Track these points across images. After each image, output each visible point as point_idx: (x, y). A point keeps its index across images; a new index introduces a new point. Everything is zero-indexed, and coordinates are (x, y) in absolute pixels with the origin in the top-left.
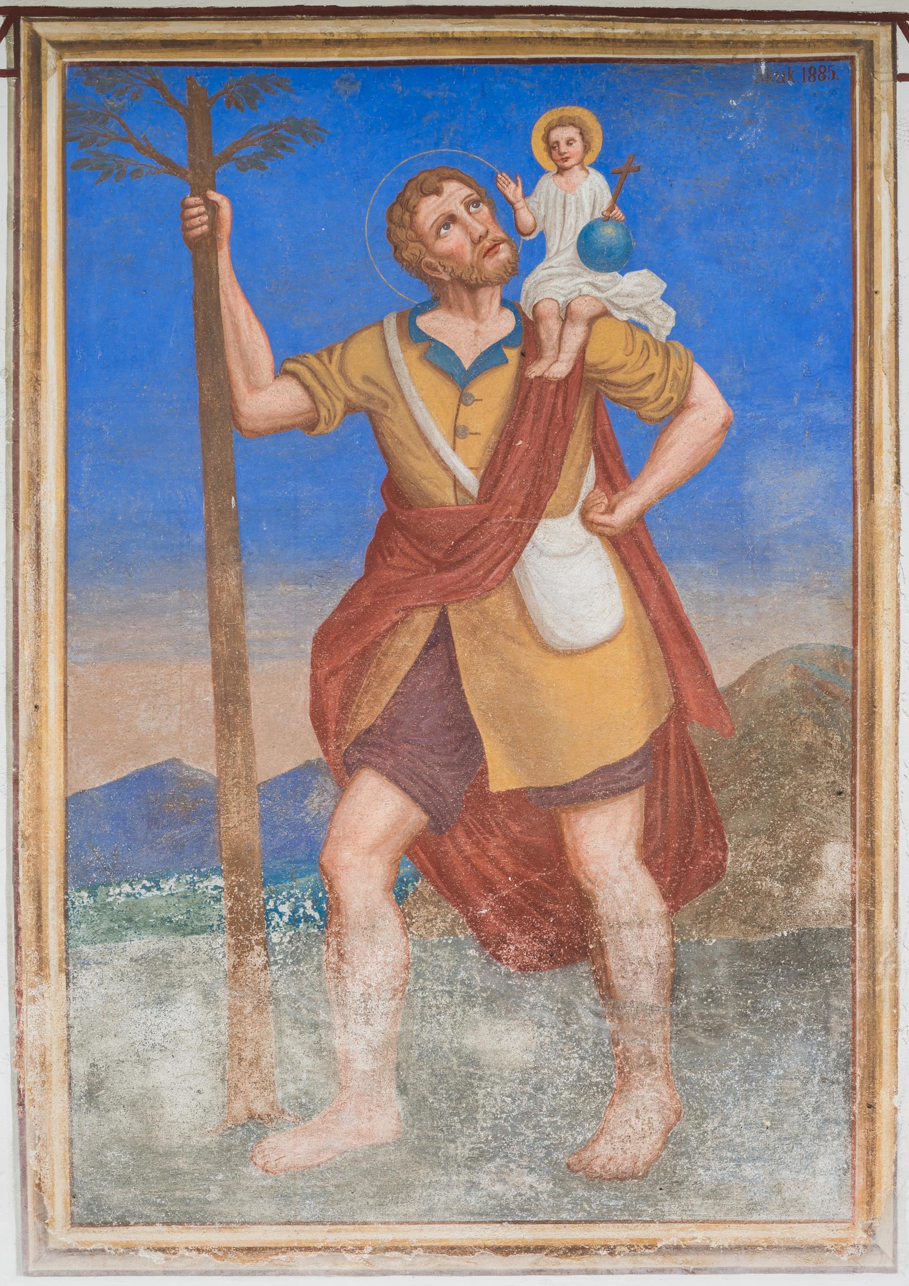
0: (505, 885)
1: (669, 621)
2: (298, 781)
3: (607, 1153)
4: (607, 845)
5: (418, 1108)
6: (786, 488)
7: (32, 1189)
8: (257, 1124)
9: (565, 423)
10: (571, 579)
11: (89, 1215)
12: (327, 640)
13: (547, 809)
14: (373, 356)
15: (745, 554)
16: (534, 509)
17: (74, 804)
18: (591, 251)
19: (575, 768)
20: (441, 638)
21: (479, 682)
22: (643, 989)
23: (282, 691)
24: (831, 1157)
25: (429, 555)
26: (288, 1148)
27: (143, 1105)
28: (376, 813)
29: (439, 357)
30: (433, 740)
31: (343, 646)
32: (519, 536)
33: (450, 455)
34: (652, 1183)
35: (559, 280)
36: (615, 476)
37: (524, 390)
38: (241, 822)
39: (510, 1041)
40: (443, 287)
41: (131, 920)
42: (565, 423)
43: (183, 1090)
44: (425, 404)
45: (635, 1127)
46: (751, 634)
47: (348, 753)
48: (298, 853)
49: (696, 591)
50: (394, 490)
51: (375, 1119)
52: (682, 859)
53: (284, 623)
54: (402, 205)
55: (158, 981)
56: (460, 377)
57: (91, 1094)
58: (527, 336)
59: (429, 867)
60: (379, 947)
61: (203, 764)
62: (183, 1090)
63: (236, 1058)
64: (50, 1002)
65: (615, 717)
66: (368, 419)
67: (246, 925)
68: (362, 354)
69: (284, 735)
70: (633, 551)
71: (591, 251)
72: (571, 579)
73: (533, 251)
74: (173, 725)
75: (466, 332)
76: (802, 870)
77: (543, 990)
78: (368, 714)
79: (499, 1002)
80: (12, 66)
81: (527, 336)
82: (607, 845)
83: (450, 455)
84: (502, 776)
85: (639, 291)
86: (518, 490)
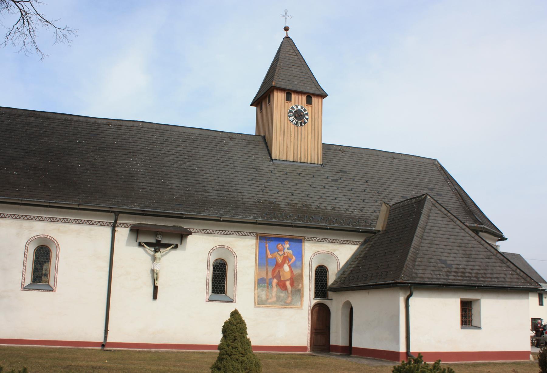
0: (282, 286)
1: (333, 209)
2: (271, 279)
3: (288, 302)
4: (288, 283)
5: (277, 299)
6: (298, 263)
7: (255, 302)
8: (268, 299)
9: (286, 259)
10: (286, 268)
11: (258, 304)
12: (273, 271)
13: (285, 281)
14: (276, 254)
15: (296, 267)
16: (284, 264)
17: (258, 280)
18: (288, 249)
19: (286, 279)
20: (279, 271)
21: (281, 274)
22: (290, 292)
23: (270, 273)
24: (300, 302)
25: (278, 266)
26: (270, 301)
27: (261, 298)
28: (275, 281)
29: (279, 254)
30: (278, 277)
31: (273, 271)
32: (283, 265)
33: (280, 260)
34: (290, 304)
35: (286, 250)
36: (289, 262)
37: (284, 257)
38: (267, 281)
39: (282, 295)
40: (280, 250)
41: (261, 286)
42: (286, 259)
43: (264, 297)
44: (278, 257)
45: (289, 300)
46: (296, 272)
47: (274, 277)
48: (271, 283)
49: (293, 269)
50: (277, 262)
51: (274, 299)
52: (292, 285)
53: (270, 269)
54: (277, 246)
55: (262, 290)
56: (280, 256)
57: (258, 297)
58: (284, 254)
59: (278, 284)
60: (275, 289)
61: (265, 278)
62: (264, 297)
63: (267, 295)
64: (256, 291)
65: (288, 276)
66: (275, 258)
67: (268, 287)
68: (275, 254)
69: (270, 276)
70: (290, 266)
71: (288, 249)
72: (286, 268)
73: (285, 249)
74: (264, 275)
75: (281, 253)
76: (298, 286)
77: (284, 292)
78: (275, 275)
79: (282, 292)
80: (113, 214)
81: (284, 254)
82: (288, 283)
83: (280, 260)
84: (282, 279)
85: (290, 251)
86: (283, 263)
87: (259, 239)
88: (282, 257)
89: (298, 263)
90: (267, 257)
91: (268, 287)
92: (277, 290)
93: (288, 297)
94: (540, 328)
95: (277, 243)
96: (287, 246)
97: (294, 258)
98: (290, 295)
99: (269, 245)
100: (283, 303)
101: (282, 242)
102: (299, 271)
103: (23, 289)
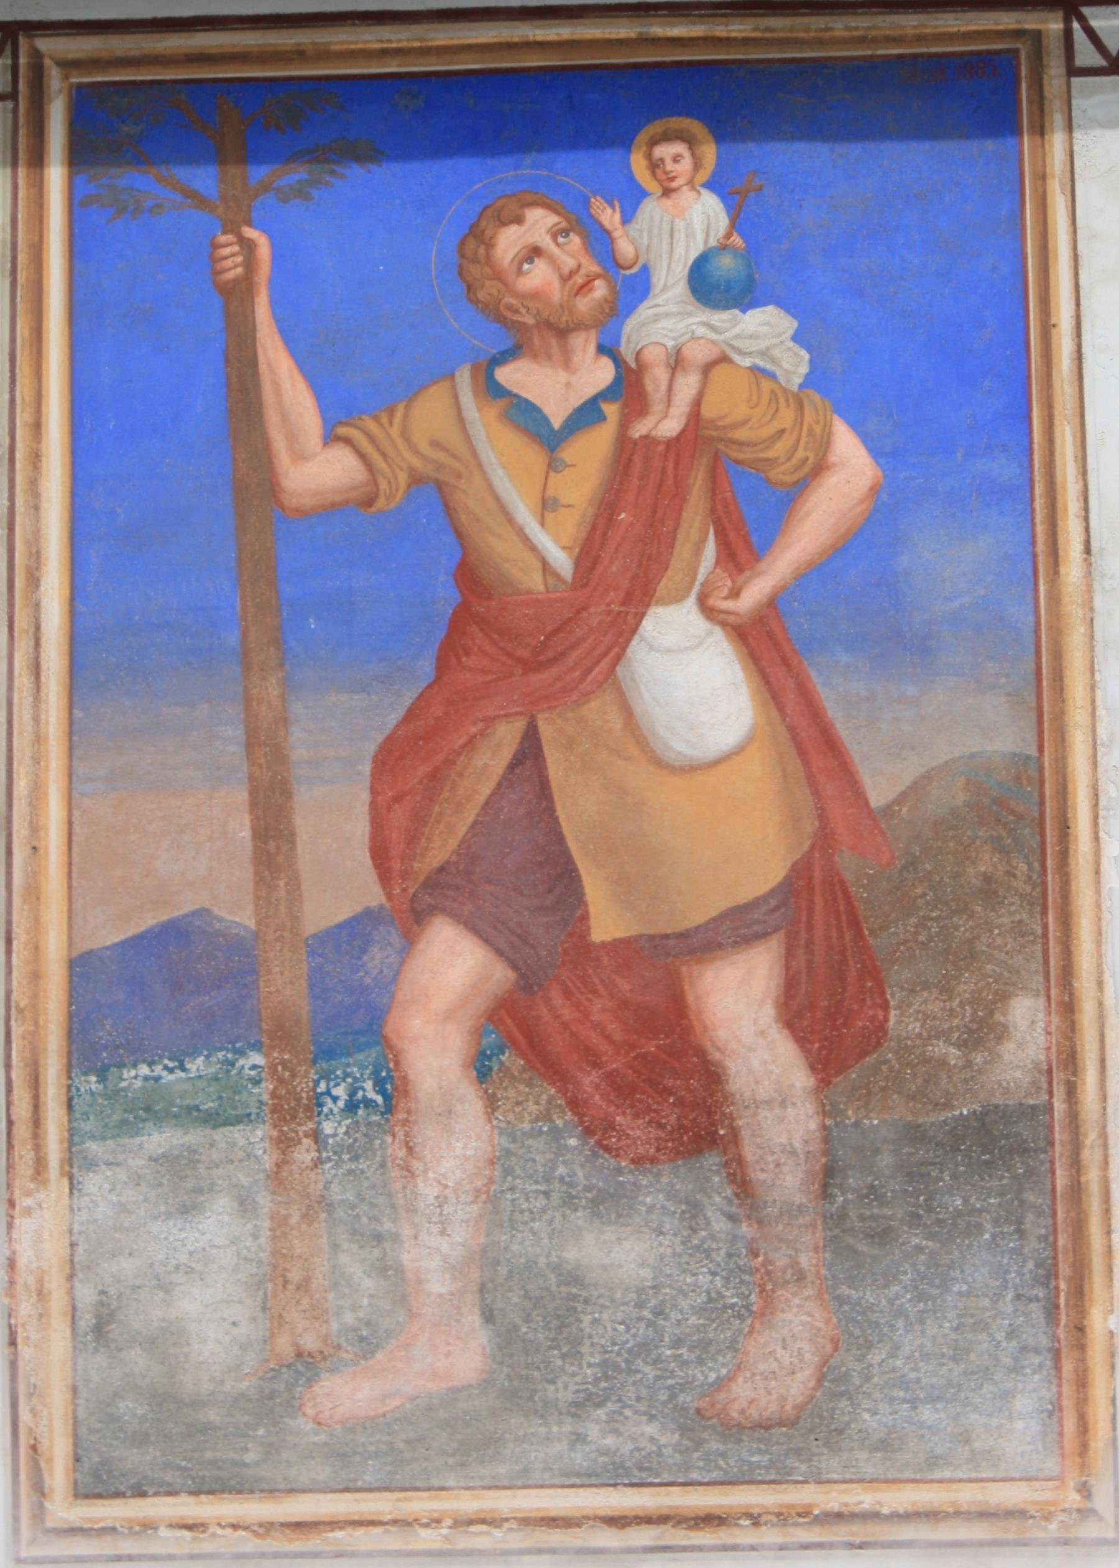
0: (611, 1062)
2: (355, 933)
3: (748, 1395)
4: (740, 1005)
5: (507, 1342)
6: (950, 563)
8: (307, 1364)
9: (681, 492)
10: (689, 678)
11: (96, 1485)
12: (390, 759)
13: (669, 958)
14: (447, 417)
15: (900, 642)
16: (640, 596)
18: (706, 286)
19: (696, 910)
20: (530, 753)
21: (578, 805)
24: (1029, 1397)
25: (515, 654)
26: (346, 1395)
27: (165, 1341)
28: (451, 970)
29: (523, 415)
30: (522, 877)
31: (409, 767)
32: (623, 629)
34: (804, 1434)
35: (667, 321)
36: (739, 553)
37: (627, 454)
38: (285, 984)
39: (621, 1254)
41: (151, 1109)
42: (681, 492)
43: (213, 1321)
44: (505, 471)
46: (914, 741)
47: (416, 899)
48: (353, 1028)
50: (470, 576)
51: (454, 1355)
52: (832, 1021)
53: (337, 741)
54: (476, 238)
55: (183, 1187)
56: (548, 438)
57: (100, 1328)
58: (630, 386)
59: (516, 1038)
60: (456, 1139)
61: (240, 915)
62: (213, 1321)
63: (280, 1282)
65: (748, 849)
66: (438, 492)
67: (292, 1112)
68: (430, 414)
69: (337, 874)
70: (765, 645)
71: (706, 286)
72: (689, 678)
73: (634, 286)
74: (200, 865)
75: (556, 385)
76: (984, 1031)
77: (658, 1190)
78: (439, 849)
79: (608, 1204)
81: (630, 386)
82: (740, 1005)
83: (538, 533)
84: (607, 923)
85: (764, 331)
87: (80, 155)
88: (593, 450)
89: (950, 563)
90: (254, 480)
91: (292, 1112)
92: (501, 1162)
93: (757, 1292)
94: (907, 1038)
95: (460, 181)
96: (681, 217)
97: (852, 467)
98: (805, 1249)
99: (287, 239)
100: (651, 1433)
101: (569, 167)
102: (1003, 736)
103: (76, 1496)
